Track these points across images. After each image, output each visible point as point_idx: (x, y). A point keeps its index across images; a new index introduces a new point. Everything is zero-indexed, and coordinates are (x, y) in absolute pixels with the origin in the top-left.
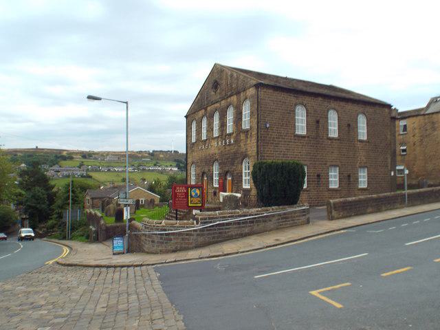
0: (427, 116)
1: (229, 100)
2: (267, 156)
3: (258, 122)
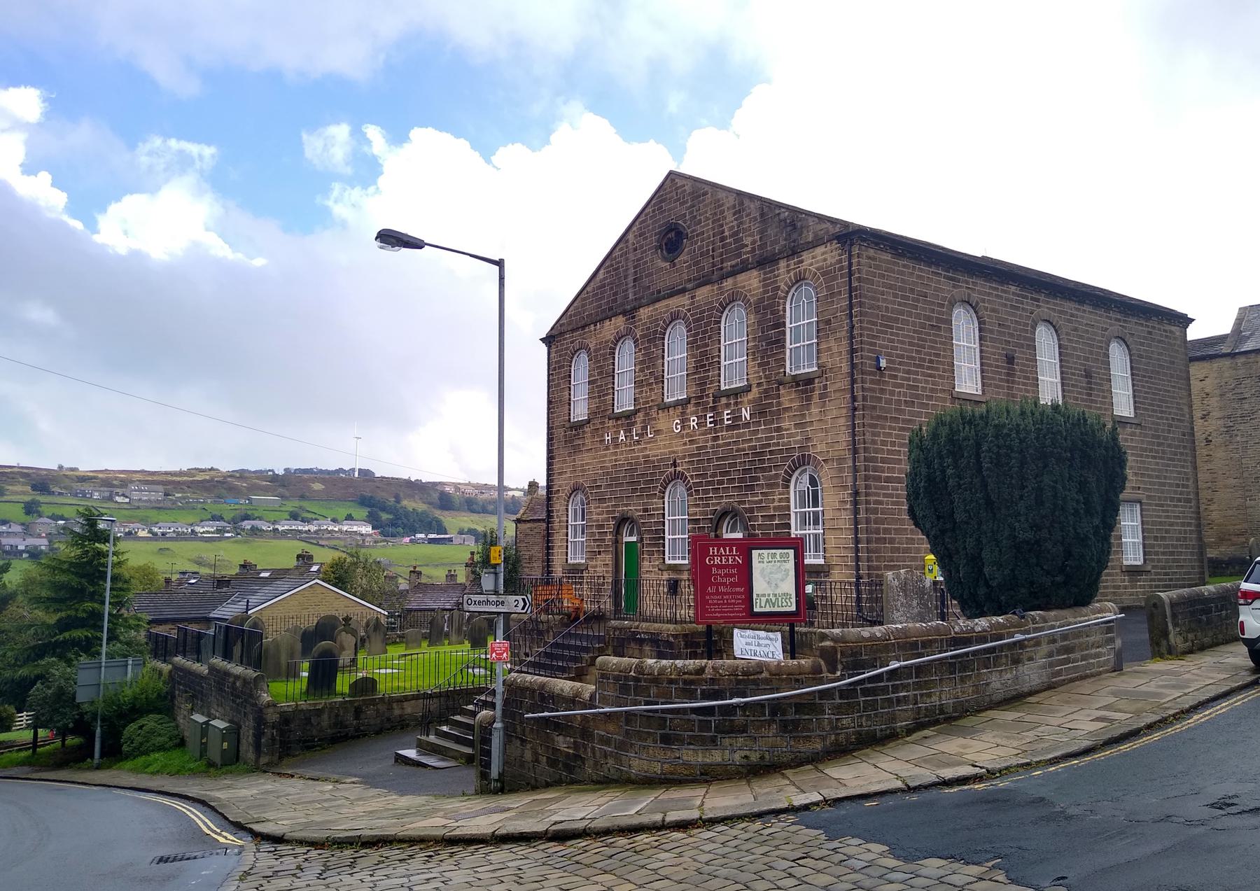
0: (1242, 360)
1: (728, 283)
2: (883, 461)
3: (852, 351)
